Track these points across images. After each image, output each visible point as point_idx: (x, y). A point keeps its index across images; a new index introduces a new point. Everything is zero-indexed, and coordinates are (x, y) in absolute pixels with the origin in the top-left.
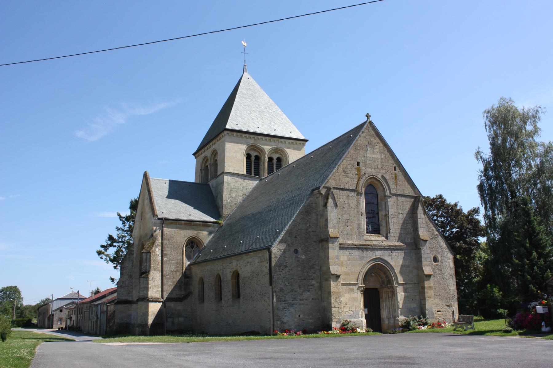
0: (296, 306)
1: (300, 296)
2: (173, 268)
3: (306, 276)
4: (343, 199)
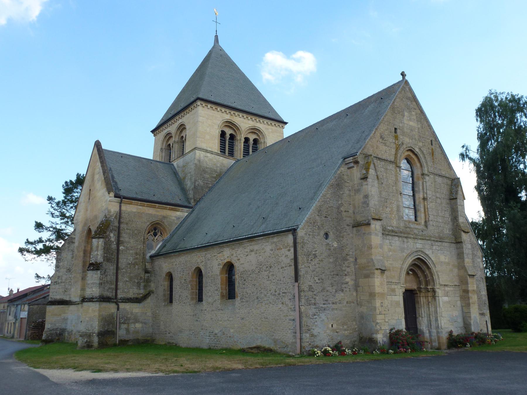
0: (328, 312)
1: (332, 298)
2: (131, 260)
3: (339, 270)
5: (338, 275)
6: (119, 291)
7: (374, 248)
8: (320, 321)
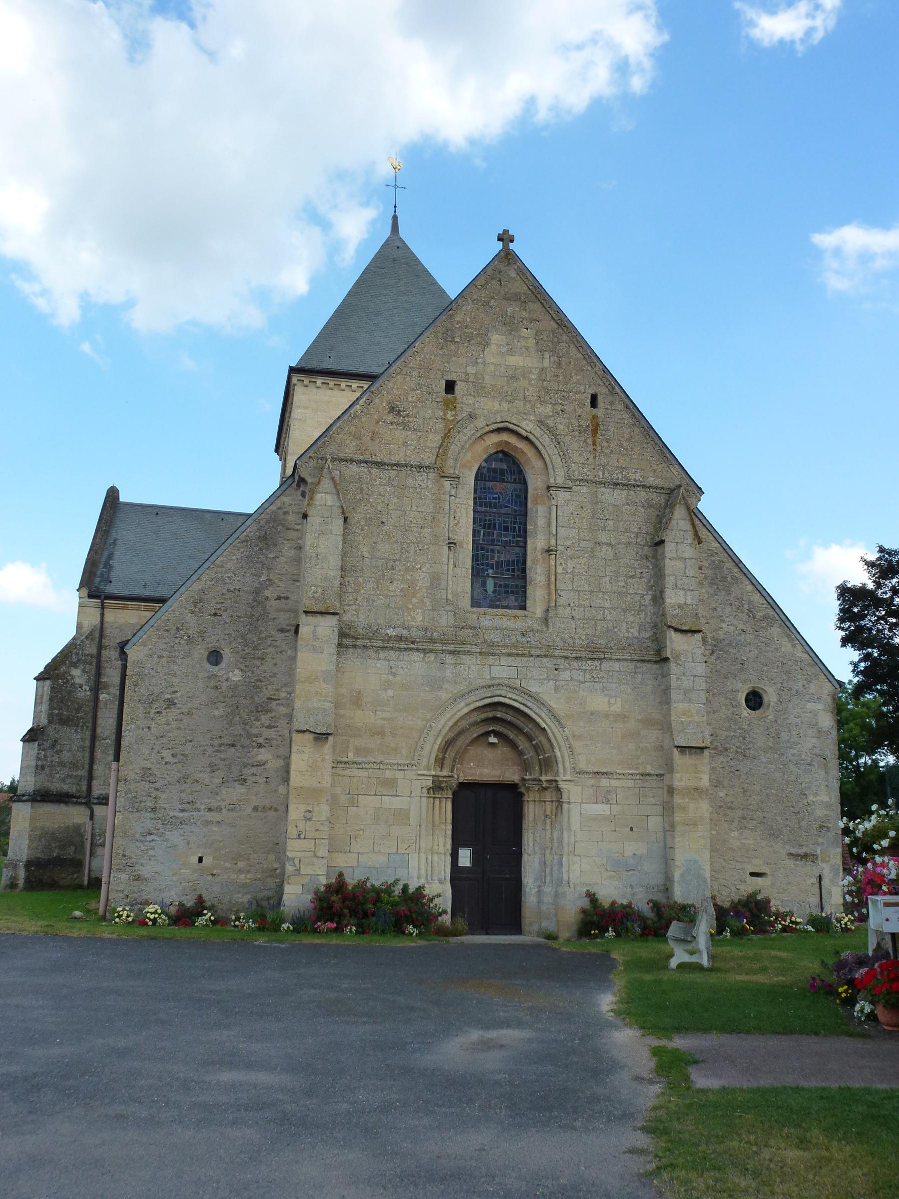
3: (241, 735)
4: (380, 494)
5: (234, 746)
6: (95, 783)
7: (303, 682)
8: (164, 847)
